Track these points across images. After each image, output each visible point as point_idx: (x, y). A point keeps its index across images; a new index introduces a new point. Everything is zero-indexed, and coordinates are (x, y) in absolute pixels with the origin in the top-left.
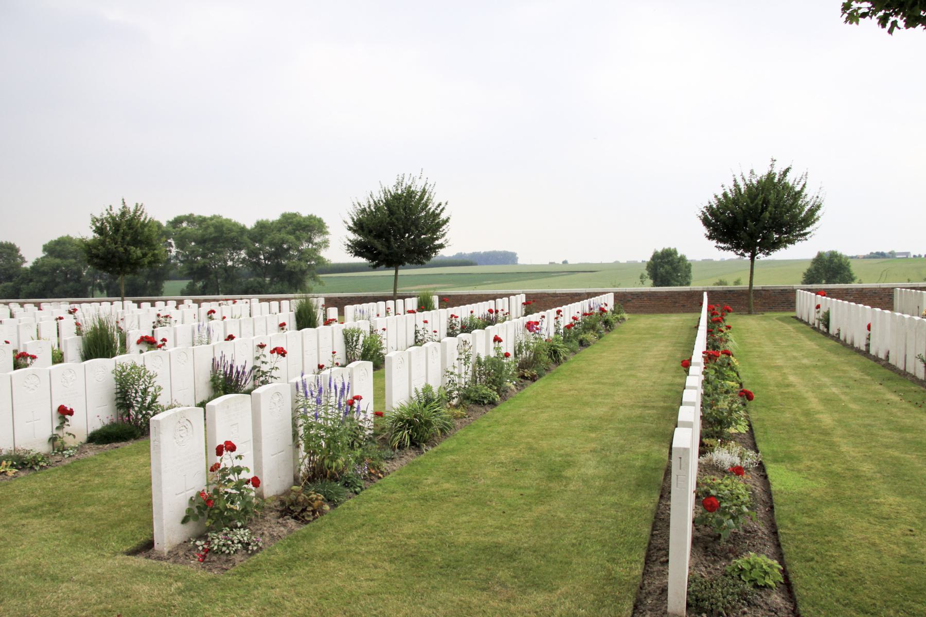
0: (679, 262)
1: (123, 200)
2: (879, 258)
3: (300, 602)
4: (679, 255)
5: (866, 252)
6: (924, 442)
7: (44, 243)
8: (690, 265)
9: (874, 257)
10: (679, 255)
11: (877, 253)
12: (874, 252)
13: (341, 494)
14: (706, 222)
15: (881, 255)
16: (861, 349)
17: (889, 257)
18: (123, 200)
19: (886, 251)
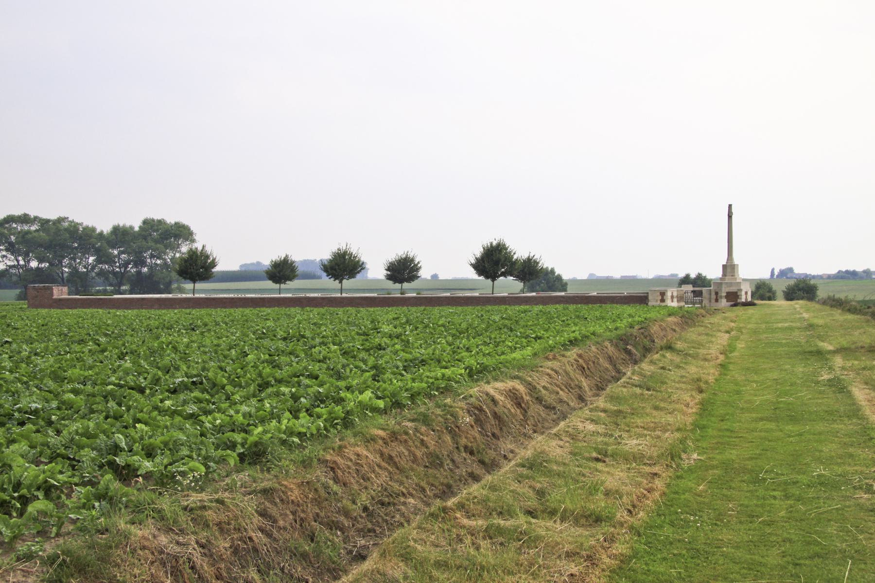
0: (555, 281)
1: (730, 206)
2: (849, 278)
3: (620, 436)
4: (556, 274)
5: (833, 271)
6: (874, 426)
7: (794, 268)
8: (566, 284)
9: (842, 278)
10: (556, 274)
11: (847, 272)
12: (844, 270)
13: (839, 446)
14: (499, 245)
15: (852, 275)
16: (18, 293)
17: (861, 278)
18: (730, 206)
19: (859, 268)
